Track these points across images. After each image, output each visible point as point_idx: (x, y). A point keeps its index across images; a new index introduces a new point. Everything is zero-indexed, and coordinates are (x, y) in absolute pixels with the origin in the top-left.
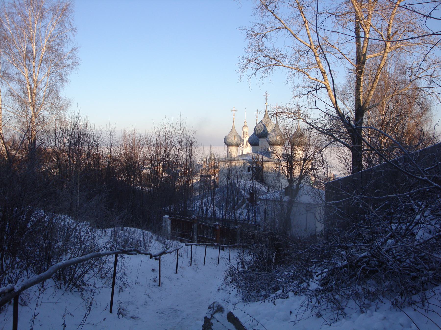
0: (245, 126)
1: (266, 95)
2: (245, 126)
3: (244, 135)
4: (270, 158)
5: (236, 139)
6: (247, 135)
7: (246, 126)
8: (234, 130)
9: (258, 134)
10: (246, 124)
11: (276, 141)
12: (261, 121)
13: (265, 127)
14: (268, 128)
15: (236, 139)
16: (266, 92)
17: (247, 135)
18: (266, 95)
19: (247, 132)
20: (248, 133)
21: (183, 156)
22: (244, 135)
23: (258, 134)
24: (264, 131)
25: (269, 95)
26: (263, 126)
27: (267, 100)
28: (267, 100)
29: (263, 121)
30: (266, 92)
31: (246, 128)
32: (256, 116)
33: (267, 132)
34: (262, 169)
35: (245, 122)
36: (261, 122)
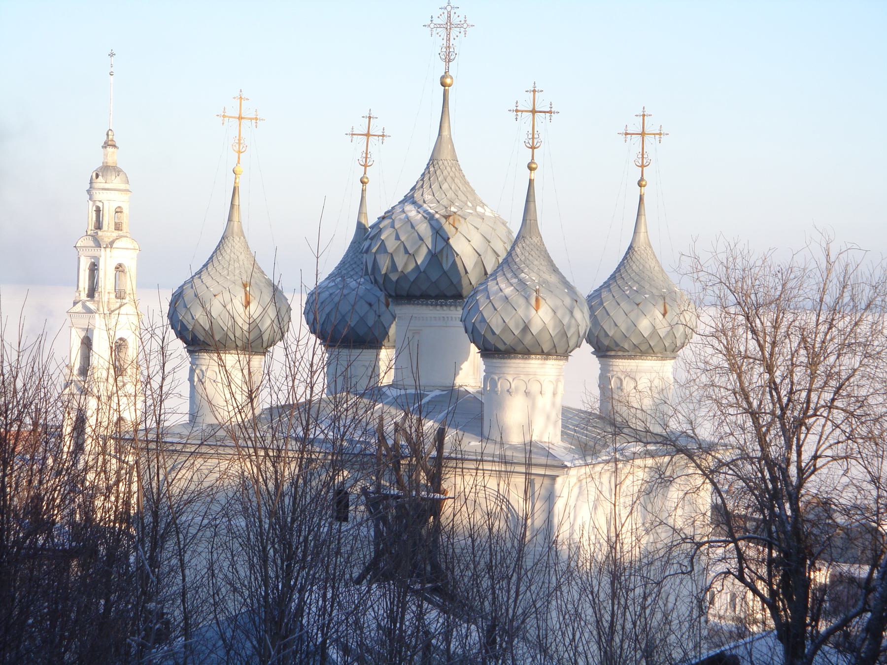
0: (106, 169)
1: (449, 26)
2: (106, 169)
3: (99, 226)
4: (483, 437)
5: (255, 309)
6: (118, 227)
7: (117, 171)
8: (235, 246)
9: (394, 277)
10: (113, 156)
11: (526, 328)
12: (407, 191)
13: (440, 234)
14: (459, 244)
15: (255, 309)
16: (449, 11)
17: (118, 227)
18: (449, 26)
19: (119, 211)
20: (125, 219)
21: (499, 525)
22: (99, 226)
23: (394, 277)
24: (434, 257)
25: (431, 25)
26: (424, 229)
27: (448, 60)
28: (448, 60)
29: (428, 197)
30: (449, 11)
31: (115, 182)
32: (359, 155)
33: (454, 263)
34: (436, 507)
35: (109, 144)
36: (409, 199)
